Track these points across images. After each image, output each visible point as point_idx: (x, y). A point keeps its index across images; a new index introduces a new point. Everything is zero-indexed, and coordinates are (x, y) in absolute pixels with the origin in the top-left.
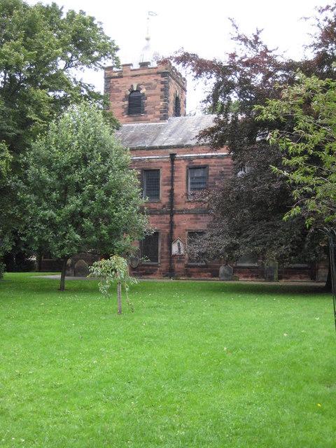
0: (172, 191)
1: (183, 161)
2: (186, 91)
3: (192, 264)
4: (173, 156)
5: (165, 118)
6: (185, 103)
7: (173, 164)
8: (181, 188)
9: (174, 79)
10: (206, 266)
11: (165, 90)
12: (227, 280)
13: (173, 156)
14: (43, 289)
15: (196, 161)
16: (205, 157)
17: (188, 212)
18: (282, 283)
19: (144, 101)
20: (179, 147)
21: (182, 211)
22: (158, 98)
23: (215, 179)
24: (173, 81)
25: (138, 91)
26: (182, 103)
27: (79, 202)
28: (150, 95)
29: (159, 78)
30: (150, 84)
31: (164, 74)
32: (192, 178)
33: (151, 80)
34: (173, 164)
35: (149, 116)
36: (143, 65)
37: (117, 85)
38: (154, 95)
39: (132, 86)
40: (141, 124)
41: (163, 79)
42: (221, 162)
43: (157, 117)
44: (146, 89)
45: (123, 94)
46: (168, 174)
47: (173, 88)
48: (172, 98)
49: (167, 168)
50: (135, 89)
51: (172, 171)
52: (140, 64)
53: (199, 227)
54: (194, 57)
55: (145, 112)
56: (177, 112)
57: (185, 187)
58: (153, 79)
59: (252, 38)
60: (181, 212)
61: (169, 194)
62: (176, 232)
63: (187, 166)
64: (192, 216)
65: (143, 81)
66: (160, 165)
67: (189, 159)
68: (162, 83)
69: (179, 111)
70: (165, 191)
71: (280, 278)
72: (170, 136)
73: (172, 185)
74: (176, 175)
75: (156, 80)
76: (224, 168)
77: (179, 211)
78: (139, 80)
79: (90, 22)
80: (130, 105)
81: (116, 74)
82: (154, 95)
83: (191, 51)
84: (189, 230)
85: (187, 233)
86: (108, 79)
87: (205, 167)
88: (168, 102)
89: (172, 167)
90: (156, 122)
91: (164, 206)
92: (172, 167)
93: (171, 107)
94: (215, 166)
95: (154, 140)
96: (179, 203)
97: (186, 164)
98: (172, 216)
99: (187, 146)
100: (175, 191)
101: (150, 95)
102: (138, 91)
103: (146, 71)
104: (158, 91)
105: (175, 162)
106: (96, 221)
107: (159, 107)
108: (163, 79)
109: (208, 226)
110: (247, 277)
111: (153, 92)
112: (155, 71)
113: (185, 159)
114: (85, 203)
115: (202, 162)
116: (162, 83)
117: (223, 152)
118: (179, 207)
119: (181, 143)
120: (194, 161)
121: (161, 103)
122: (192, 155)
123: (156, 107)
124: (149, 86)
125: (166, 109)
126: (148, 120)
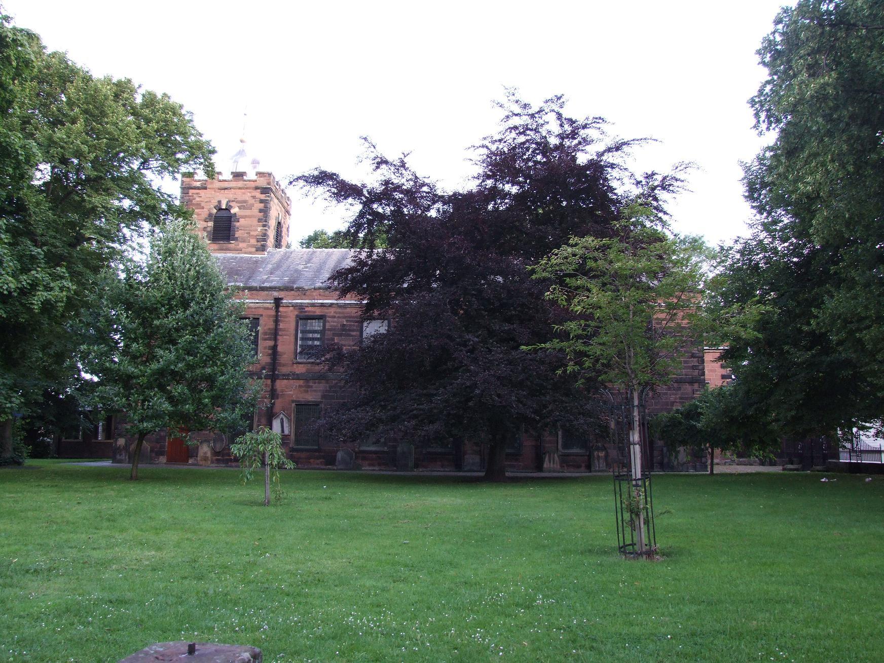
0: (274, 348)
1: (291, 308)
2: (289, 215)
3: (299, 447)
4: (278, 301)
5: (263, 248)
6: (288, 230)
7: (277, 311)
8: (286, 346)
9: (278, 199)
10: (318, 451)
11: (265, 211)
12: (389, 471)
13: (278, 301)
14: (100, 477)
15: (250, 304)
16: (322, 305)
17: (297, 377)
18: (415, 473)
19: (235, 223)
20: (287, 289)
21: (288, 375)
22: (254, 222)
23: (334, 335)
24: (276, 201)
25: (228, 209)
26: (284, 230)
27: (172, 356)
28: (245, 217)
29: (258, 194)
30: (245, 202)
31: (265, 190)
32: (302, 332)
33: (247, 196)
34: (277, 311)
35: (241, 245)
36: (238, 175)
37: (198, 199)
38: (249, 217)
39: (220, 202)
40: (229, 255)
41: (263, 197)
42: (343, 313)
43: (253, 246)
44: (240, 208)
45: (204, 213)
46: (271, 325)
47: (275, 210)
48: (273, 223)
49: (269, 316)
50: (224, 207)
51: (276, 321)
52: (232, 173)
53: (310, 397)
54: (331, 176)
55: (236, 239)
56: (278, 244)
57: (293, 344)
58: (249, 195)
59: (397, 163)
60: (286, 377)
61: (270, 352)
62: (279, 404)
63: (297, 316)
64: (301, 382)
65: (235, 196)
66: (261, 312)
67: (301, 307)
68: (261, 201)
69: (280, 241)
70: (265, 348)
71: (416, 466)
72: (271, 273)
73: (276, 340)
74: (281, 326)
75: (254, 197)
76: (347, 321)
77: (284, 375)
78: (230, 195)
79: (174, 110)
80: (215, 228)
81: (198, 184)
82: (249, 217)
83: (330, 169)
84: (296, 401)
85: (293, 405)
86: (185, 189)
87: (321, 318)
88: (269, 228)
89: (277, 316)
90: (251, 253)
91: (264, 368)
92: (277, 316)
93: (272, 234)
94: (334, 317)
95: (250, 278)
96: (284, 365)
97: (296, 313)
98: (273, 382)
99: (298, 289)
100: (279, 349)
101: (245, 217)
102: (228, 209)
103: (240, 184)
104: (255, 211)
105: (281, 309)
106: (193, 386)
107: (256, 233)
108: (263, 197)
109: (324, 397)
110: (373, 465)
111: (247, 212)
112: (253, 185)
113: (295, 306)
114: (179, 359)
115: (318, 311)
116: (261, 201)
117: (350, 300)
118: (284, 370)
119: (287, 285)
120: (307, 309)
121: (259, 229)
122: (305, 301)
123: (252, 233)
124: (243, 205)
125: (264, 237)
126: (239, 250)
